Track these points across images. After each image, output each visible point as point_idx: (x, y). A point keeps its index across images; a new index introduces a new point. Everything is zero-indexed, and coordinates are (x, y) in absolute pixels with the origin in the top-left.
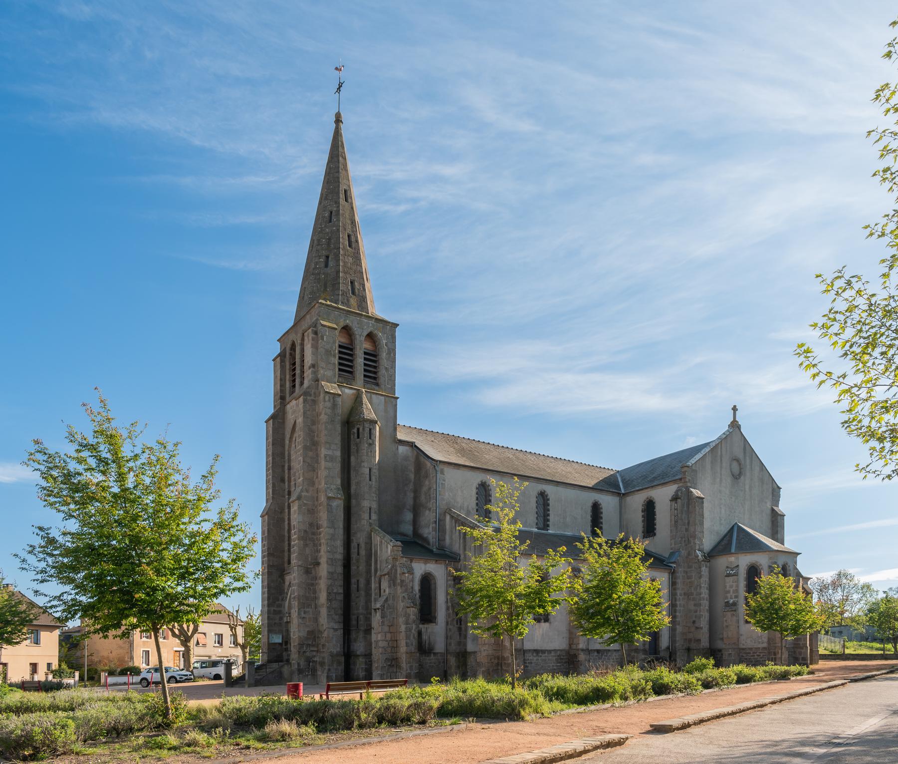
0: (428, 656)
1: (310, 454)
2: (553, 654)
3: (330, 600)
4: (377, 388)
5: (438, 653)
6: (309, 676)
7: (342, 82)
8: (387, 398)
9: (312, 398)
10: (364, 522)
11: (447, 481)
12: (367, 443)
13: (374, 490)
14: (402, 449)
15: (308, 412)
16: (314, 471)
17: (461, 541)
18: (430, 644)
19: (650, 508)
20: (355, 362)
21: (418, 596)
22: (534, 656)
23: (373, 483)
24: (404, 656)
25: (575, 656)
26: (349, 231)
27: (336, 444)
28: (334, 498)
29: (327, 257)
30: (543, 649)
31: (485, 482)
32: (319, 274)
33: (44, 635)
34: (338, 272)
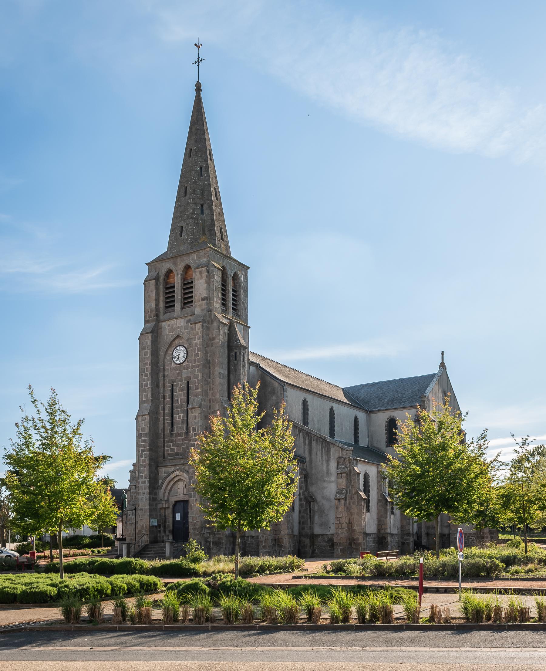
7: (202, 57)
17: (307, 447)
19: (392, 424)
24: (287, 537)
25: (384, 538)
29: (202, 206)
32: (197, 219)
34: (213, 220)
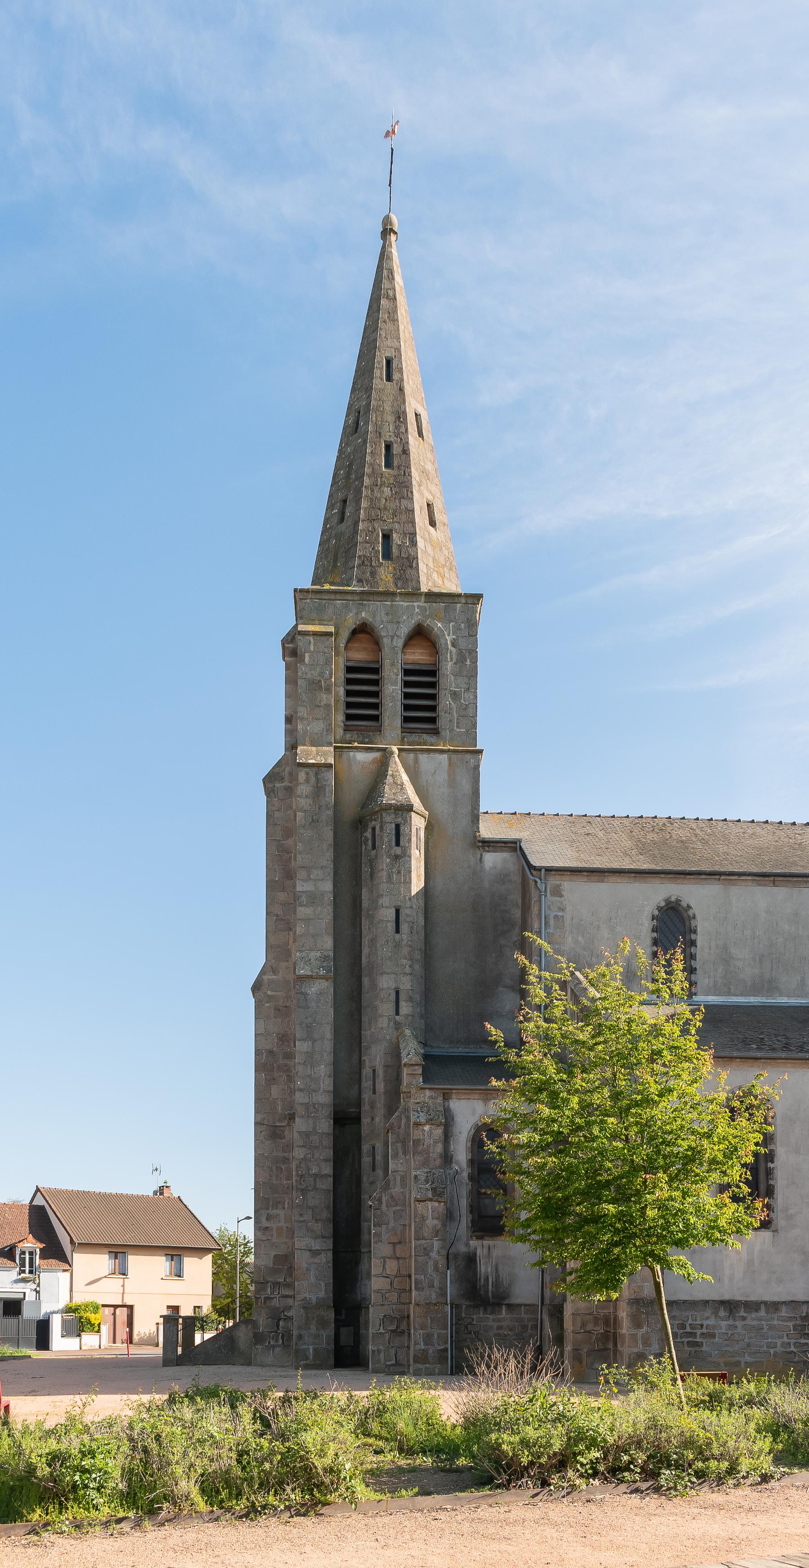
0: (492, 1313)
1: (281, 896)
2: (784, 1312)
3: (302, 1190)
4: (433, 739)
5: (520, 1305)
6: (277, 1350)
8: (454, 757)
9: (286, 784)
10: (383, 1022)
11: (569, 908)
12: (389, 856)
13: (405, 951)
14: (491, 859)
15: (277, 814)
16: (290, 929)
18: (497, 1283)
20: (440, 708)
21: (465, 1174)
22: (722, 1319)
23: (404, 937)
26: (388, 435)
27: (322, 867)
28: (310, 977)
29: (345, 501)
30: (753, 1298)
31: (678, 901)
33: (190, 1263)
